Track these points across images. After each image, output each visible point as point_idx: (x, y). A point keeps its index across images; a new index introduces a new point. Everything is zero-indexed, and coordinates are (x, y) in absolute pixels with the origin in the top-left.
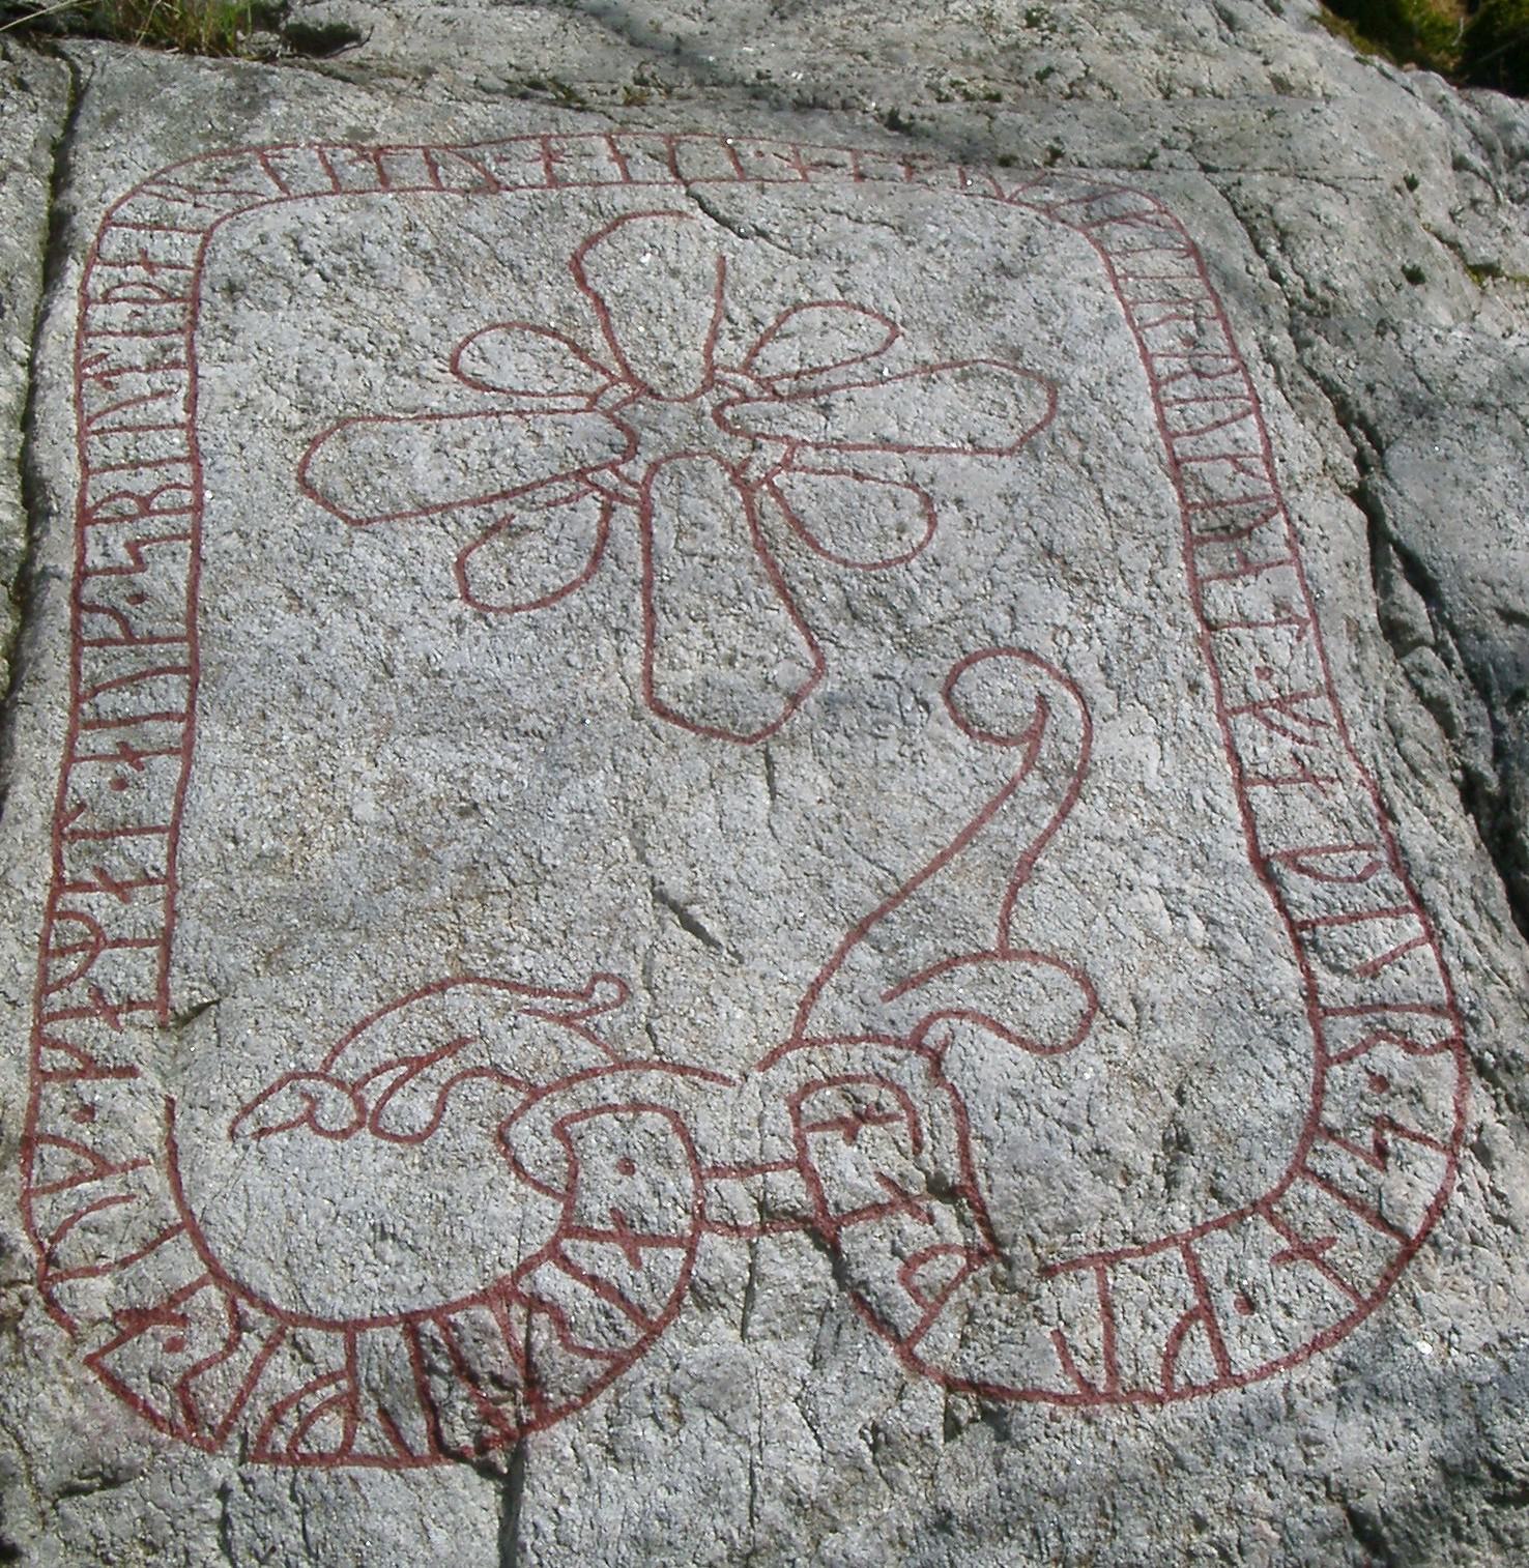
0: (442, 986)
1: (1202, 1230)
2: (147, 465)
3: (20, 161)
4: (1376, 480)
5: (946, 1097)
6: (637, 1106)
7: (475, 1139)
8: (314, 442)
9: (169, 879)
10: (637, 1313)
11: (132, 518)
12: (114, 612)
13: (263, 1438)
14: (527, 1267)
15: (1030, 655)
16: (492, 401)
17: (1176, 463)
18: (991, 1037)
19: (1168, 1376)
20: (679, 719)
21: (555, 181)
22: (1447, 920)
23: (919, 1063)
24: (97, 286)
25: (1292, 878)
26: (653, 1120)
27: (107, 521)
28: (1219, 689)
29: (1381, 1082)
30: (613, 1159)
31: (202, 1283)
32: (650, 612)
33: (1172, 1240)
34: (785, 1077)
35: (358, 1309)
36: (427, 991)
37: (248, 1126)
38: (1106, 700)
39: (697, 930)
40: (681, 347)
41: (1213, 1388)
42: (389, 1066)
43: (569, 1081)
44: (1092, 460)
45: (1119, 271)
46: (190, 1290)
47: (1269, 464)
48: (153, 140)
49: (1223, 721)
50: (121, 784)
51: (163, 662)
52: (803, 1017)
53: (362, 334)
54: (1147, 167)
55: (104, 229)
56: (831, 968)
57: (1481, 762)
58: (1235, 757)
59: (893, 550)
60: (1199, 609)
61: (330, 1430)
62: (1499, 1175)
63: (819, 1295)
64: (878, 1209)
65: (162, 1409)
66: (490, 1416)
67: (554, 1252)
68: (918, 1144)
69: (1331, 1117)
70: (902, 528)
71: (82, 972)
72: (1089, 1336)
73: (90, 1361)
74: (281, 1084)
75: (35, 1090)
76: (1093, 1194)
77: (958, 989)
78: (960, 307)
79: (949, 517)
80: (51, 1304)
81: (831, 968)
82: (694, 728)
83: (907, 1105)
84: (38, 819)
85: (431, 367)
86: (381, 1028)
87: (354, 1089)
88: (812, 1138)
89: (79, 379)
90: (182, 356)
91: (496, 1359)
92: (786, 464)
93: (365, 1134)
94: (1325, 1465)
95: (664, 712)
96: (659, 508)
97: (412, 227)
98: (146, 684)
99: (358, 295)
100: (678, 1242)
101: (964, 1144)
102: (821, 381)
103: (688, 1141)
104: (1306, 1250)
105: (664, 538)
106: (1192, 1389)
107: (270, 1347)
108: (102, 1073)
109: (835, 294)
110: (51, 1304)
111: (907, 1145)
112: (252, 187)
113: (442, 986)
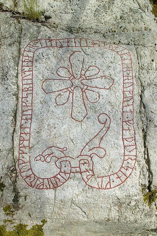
0: (52, 147)
1: (111, 175)
2: (28, 84)
4: (143, 95)
5: (92, 162)
6: (67, 161)
8: (43, 82)
10: (65, 179)
11: (27, 91)
12: (25, 103)
15: (106, 114)
16: (60, 78)
19: (106, 187)
20: (74, 119)
21: (68, 46)
22: (138, 147)
23: (90, 158)
26: (68, 162)
27: (24, 91)
28: (123, 119)
29: (128, 163)
30: (64, 166)
32: (72, 106)
33: (108, 176)
34: (79, 159)
35: (44, 178)
37: (36, 160)
38: (112, 120)
41: (109, 189)
42: (47, 155)
44: (116, 91)
45: (123, 63)
46: (31, 175)
47: (133, 92)
48: (29, 38)
49: (122, 123)
50: (26, 123)
51: (29, 109)
52: (81, 153)
53: (48, 67)
56: (84, 148)
57: (145, 127)
58: (123, 127)
59: (95, 101)
60: (123, 110)
61: (42, 187)
64: (85, 172)
67: (59, 174)
68: (89, 166)
71: (23, 143)
72: (100, 184)
73: (24, 179)
74: (38, 156)
76: (103, 171)
77: (94, 151)
78: (106, 68)
79: (101, 97)
80: (21, 175)
81: (84, 148)
82: (75, 120)
83: (89, 162)
84: (19, 126)
86: (46, 151)
87: (44, 157)
88: (81, 165)
90: (32, 70)
92: (86, 89)
94: (116, 195)
95: (72, 118)
97: (54, 53)
99: (48, 62)
100: (69, 174)
102: (90, 78)
103: (70, 165)
104: (119, 177)
105: (74, 98)
106: (108, 189)
107: (37, 180)
108: (24, 153)
109: (94, 65)
111: (88, 166)
112: (38, 46)
113: (52, 147)
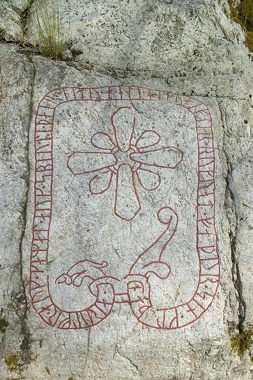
1: (178, 306)
3: (26, 89)
4: (230, 177)
6: (107, 283)
7: (86, 287)
8: (70, 157)
9: (48, 239)
10: (105, 314)
11: (43, 171)
12: (40, 190)
13: (59, 326)
14: (92, 306)
15: (171, 209)
17: (199, 172)
18: (155, 276)
19: (170, 326)
20: (119, 216)
22: (222, 261)
23: (145, 279)
25: (201, 252)
26: (109, 286)
29: (206, 287)
31: (51, 305)
34: (127, 281)
35: (70, 310)
36: (81, 262)
38: (180, 217)
40: (126, 140)
41: (176, 328)
43: (98, 279)
46: (50, 306)
47: (214, 173)
48: (46, 86)
50: (41, 222)
51: (47, 200)
52: (131, 270)
54: (207, 96)
55: (38, 107)
57: (233, 230)
58: (198, 229)
59: (153, 187)
60: (197, 201)
61: (67, 326)
62: (219, 300)
63: (128, 311)
65: (47, 321)
67: (95, 304)
70: (155, 183)
71: (36, 255)
72: (161, 320)
73: (39, 313)
75: (31, 274)
77: (151, 268)
79: (163, 181)
80: (33, 306)
86: (74, 268)
87: (71, 277)
88: (130, 290)
89: (35, 141)
92: (139, 168)
93: (72, 285)
95: (117, 215)
96: (119, 176)
100: (111, 304)
101: (149, 292)
104: (191, 310)
106: (173, 328)
108: (39, 272)
109: (151, 129)
110: (33, 306)
111: (142, 292)
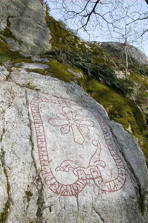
7: (72, 172)
14: (77, 181)
23: (97, 168)
24: (32, 106)
34: (89, 168)
35: (66, 184)
39: (81, 158)
46: (55, 182)
64: (96, 178)
66: (75, 192)
67: (78, 180)
69: (119, 173)
73: (49, 188)
85: (55, 115)
91: (75, 188)
98: (42, 136)
100: (85, 180)
105: (73, 130)
108: (45, 166)
